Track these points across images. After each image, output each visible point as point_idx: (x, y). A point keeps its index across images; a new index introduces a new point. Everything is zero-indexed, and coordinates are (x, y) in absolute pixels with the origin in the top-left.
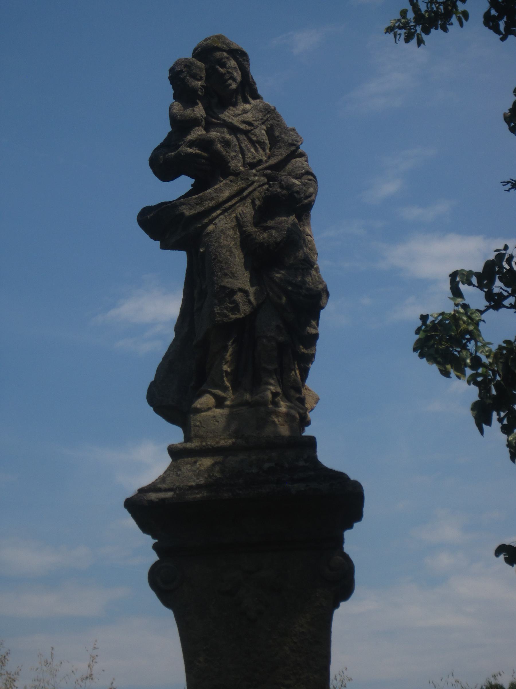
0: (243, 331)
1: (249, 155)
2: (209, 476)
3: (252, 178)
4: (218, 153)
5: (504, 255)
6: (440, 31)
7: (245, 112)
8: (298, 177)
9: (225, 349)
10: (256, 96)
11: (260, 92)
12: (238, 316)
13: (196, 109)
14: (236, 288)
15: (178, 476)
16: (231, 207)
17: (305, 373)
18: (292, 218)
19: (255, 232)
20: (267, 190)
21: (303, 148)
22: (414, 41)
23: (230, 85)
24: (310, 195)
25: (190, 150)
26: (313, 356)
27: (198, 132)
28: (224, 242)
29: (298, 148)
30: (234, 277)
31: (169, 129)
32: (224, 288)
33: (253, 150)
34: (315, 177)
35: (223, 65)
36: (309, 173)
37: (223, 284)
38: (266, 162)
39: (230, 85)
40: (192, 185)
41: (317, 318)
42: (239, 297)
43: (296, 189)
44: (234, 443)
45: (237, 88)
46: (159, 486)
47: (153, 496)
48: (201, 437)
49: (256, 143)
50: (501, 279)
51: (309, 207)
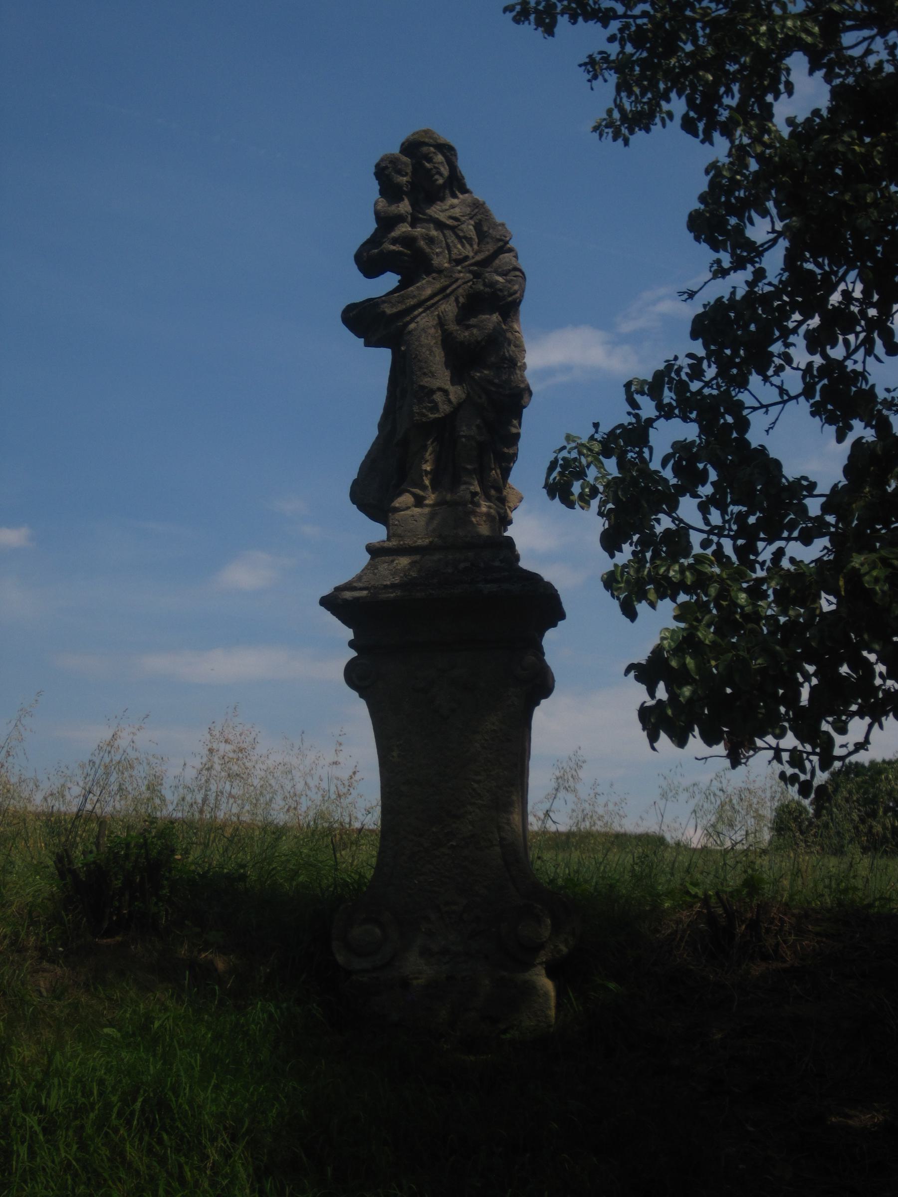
0: (443, 430)
1: (455, 251)
2: (405, 575)
3: (457, 275)
4: (421, 251)
5: (673, 365)
6: (643, 132)
7: (453, 207)
8: (504, 274)
9: (425, 448)
10: (464, 190)
11: (469, 186)
12: (436, 416)
13: (401, 205)
14: (435, 388)
15: (375, 574)
16: (433, 305)
17: (506, 473)
18: (495, 317)
19: (457, 330)
20: (471, 287)
21: (512, 244)
22: (620, 141)
23: (437, 180)
24: (515, 292)
26: (515, 455)
27: (404, 228)
28: (424, 340)
29: (507, 243)
30: (433, 376)
31: (374, 226)
32: (423, 388)
33: (459, 246)
34: (523, 273)
35: (430, 160)
36: (516, 269)
37: (422, 383)
38: (473, 258)
39: (437, 180)
40: (399, 281)
41: (519, 416)
42: (438, 397)
43: (498, 286)
44: (431, 543)
45: (445, 183)
46: (355, 584)
47: (348, 595)
48: (400, 536)
49: (464, 239)
50: (670, 389)
51: (516, 304)
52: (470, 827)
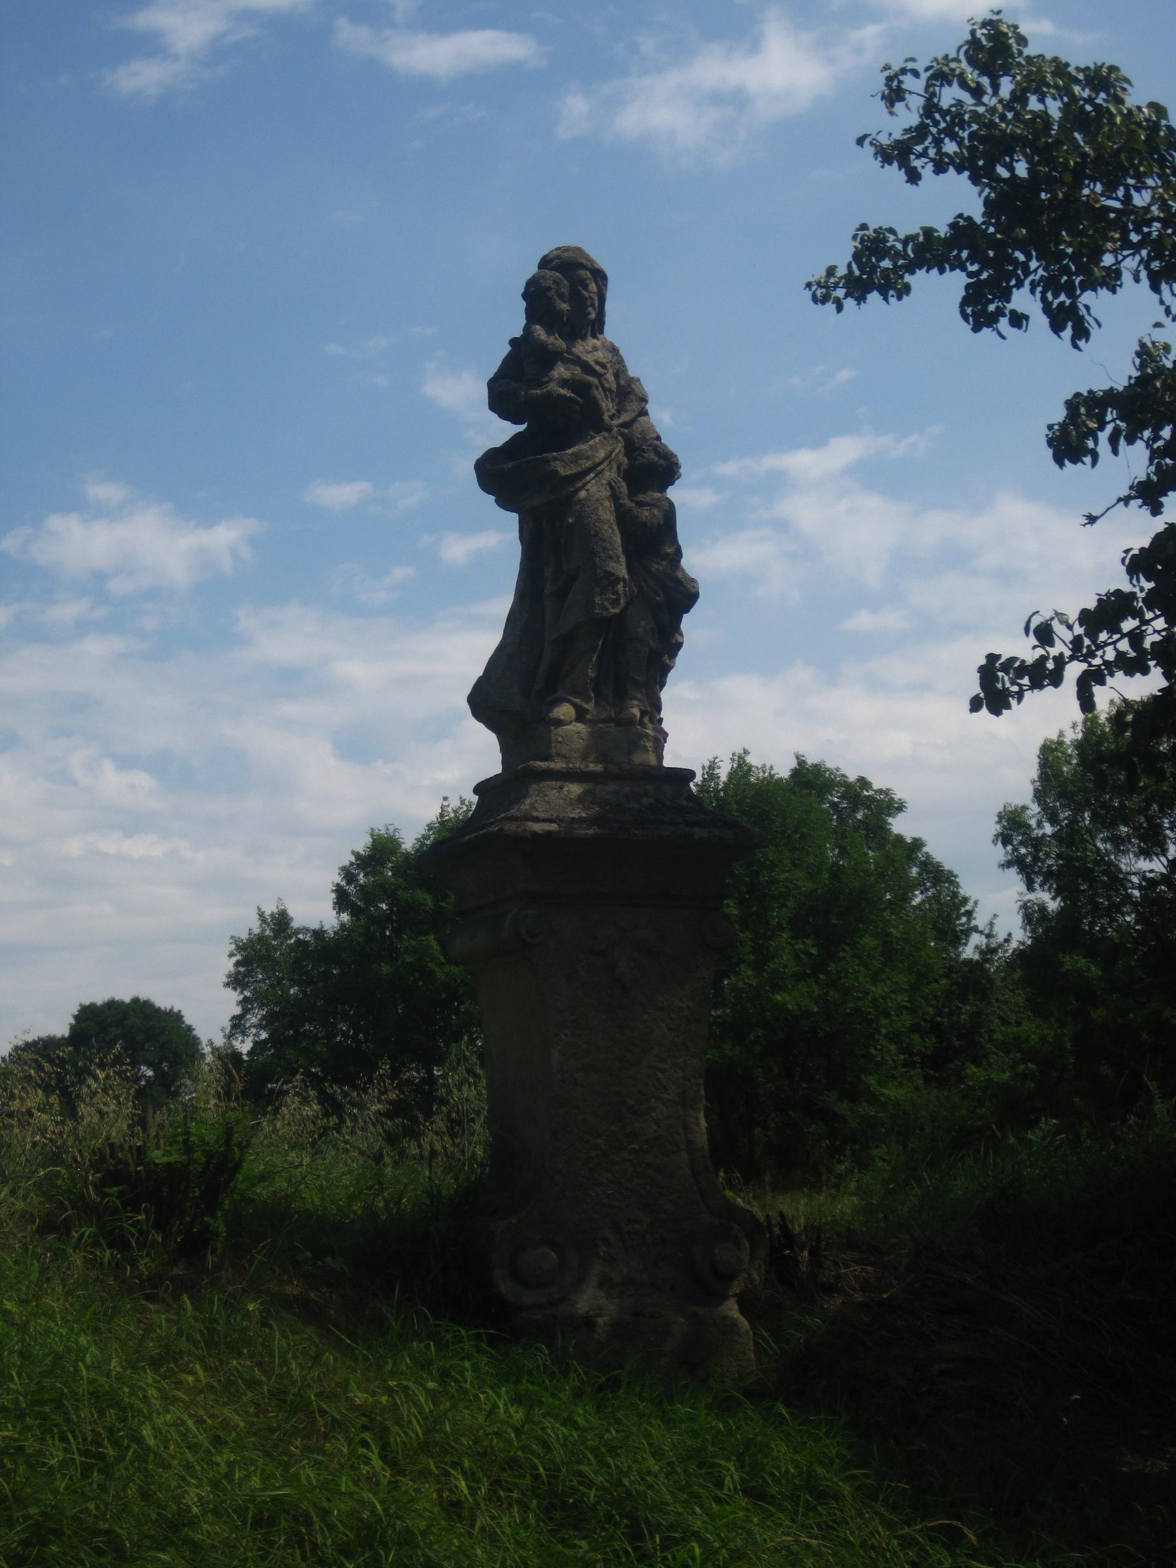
25: (564, 392)
35: (586, 287)
48: (564, 756)
52: (654, 1127)
